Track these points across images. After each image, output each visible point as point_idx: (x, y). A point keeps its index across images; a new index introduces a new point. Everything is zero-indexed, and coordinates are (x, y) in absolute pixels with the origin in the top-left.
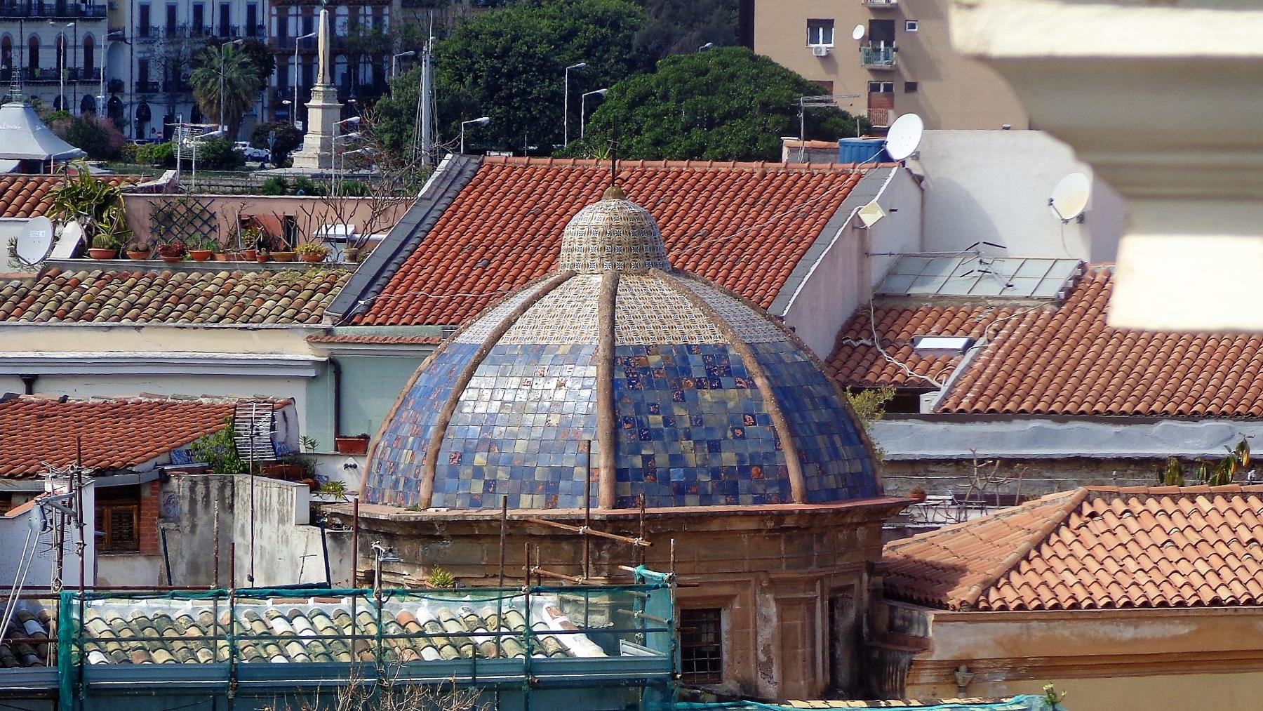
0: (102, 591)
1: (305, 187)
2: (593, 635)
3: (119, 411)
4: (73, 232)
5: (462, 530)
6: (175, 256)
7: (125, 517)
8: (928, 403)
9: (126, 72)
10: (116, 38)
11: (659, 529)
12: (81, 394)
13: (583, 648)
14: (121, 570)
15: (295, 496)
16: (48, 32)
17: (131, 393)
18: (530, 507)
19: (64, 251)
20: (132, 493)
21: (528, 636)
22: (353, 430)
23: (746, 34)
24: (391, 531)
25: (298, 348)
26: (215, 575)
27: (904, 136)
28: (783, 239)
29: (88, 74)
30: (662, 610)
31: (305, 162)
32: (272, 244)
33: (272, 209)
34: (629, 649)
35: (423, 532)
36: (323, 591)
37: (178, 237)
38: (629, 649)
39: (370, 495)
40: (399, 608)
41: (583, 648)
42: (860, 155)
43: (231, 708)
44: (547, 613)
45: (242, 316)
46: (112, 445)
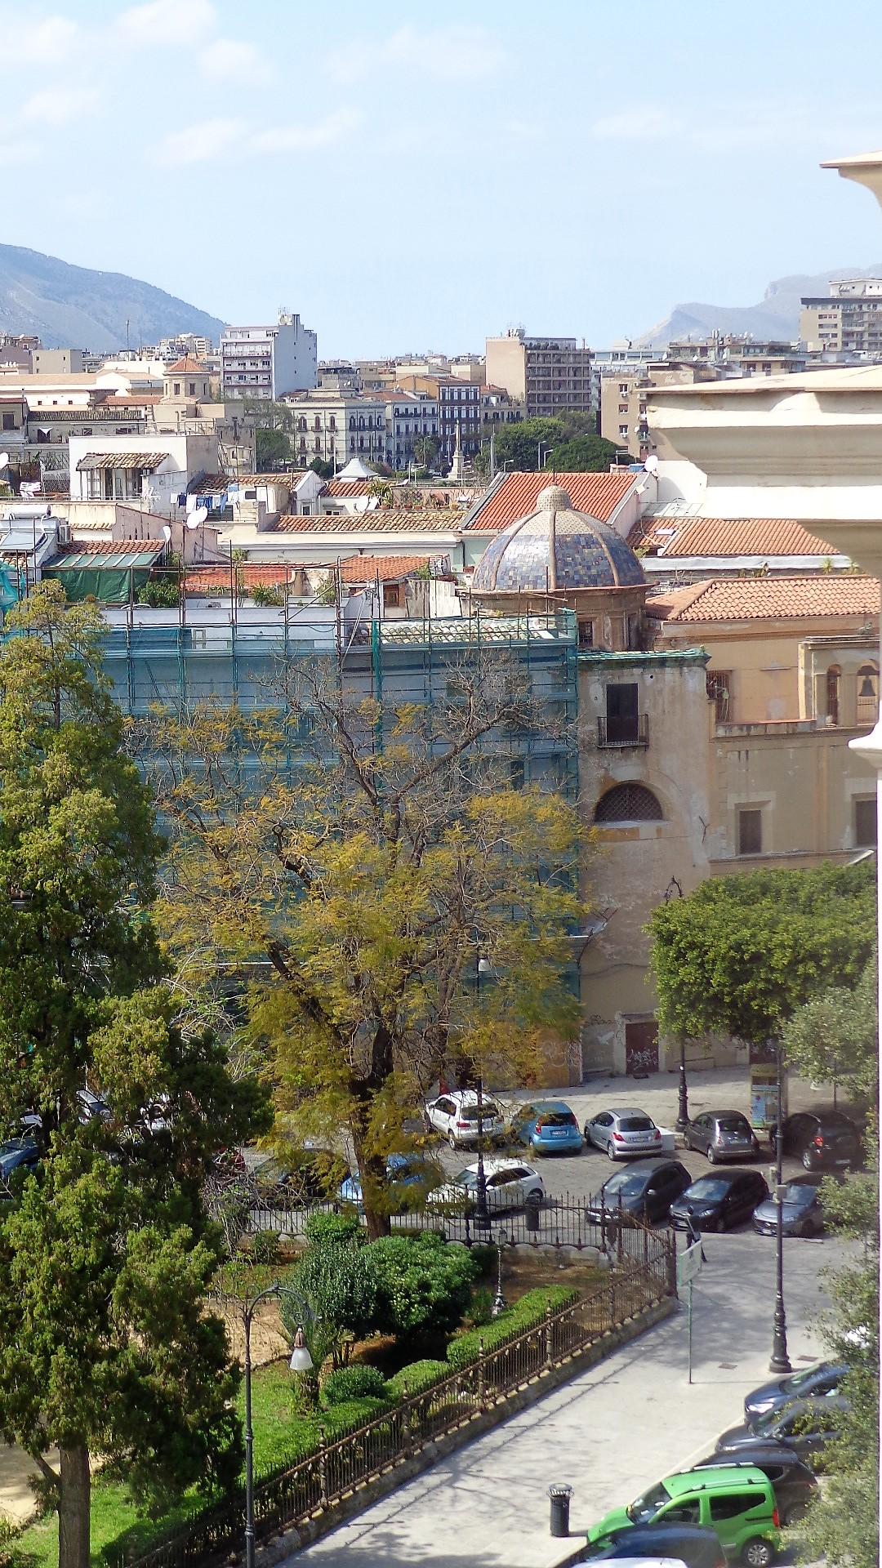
4: (375, 501)
8: (660, 552)
9: (394, 449)
10: (389, 436)
11: (571, 595)
13: (547, 635)
14: (393, 612)
16: (366, 435)
19: (372, 507)
28: (29, 525)
30: (572, 622)
34: (562, 635)
35: (493, 598)
38: (562, 635)
41: (547, 635)
44: (534, 624)
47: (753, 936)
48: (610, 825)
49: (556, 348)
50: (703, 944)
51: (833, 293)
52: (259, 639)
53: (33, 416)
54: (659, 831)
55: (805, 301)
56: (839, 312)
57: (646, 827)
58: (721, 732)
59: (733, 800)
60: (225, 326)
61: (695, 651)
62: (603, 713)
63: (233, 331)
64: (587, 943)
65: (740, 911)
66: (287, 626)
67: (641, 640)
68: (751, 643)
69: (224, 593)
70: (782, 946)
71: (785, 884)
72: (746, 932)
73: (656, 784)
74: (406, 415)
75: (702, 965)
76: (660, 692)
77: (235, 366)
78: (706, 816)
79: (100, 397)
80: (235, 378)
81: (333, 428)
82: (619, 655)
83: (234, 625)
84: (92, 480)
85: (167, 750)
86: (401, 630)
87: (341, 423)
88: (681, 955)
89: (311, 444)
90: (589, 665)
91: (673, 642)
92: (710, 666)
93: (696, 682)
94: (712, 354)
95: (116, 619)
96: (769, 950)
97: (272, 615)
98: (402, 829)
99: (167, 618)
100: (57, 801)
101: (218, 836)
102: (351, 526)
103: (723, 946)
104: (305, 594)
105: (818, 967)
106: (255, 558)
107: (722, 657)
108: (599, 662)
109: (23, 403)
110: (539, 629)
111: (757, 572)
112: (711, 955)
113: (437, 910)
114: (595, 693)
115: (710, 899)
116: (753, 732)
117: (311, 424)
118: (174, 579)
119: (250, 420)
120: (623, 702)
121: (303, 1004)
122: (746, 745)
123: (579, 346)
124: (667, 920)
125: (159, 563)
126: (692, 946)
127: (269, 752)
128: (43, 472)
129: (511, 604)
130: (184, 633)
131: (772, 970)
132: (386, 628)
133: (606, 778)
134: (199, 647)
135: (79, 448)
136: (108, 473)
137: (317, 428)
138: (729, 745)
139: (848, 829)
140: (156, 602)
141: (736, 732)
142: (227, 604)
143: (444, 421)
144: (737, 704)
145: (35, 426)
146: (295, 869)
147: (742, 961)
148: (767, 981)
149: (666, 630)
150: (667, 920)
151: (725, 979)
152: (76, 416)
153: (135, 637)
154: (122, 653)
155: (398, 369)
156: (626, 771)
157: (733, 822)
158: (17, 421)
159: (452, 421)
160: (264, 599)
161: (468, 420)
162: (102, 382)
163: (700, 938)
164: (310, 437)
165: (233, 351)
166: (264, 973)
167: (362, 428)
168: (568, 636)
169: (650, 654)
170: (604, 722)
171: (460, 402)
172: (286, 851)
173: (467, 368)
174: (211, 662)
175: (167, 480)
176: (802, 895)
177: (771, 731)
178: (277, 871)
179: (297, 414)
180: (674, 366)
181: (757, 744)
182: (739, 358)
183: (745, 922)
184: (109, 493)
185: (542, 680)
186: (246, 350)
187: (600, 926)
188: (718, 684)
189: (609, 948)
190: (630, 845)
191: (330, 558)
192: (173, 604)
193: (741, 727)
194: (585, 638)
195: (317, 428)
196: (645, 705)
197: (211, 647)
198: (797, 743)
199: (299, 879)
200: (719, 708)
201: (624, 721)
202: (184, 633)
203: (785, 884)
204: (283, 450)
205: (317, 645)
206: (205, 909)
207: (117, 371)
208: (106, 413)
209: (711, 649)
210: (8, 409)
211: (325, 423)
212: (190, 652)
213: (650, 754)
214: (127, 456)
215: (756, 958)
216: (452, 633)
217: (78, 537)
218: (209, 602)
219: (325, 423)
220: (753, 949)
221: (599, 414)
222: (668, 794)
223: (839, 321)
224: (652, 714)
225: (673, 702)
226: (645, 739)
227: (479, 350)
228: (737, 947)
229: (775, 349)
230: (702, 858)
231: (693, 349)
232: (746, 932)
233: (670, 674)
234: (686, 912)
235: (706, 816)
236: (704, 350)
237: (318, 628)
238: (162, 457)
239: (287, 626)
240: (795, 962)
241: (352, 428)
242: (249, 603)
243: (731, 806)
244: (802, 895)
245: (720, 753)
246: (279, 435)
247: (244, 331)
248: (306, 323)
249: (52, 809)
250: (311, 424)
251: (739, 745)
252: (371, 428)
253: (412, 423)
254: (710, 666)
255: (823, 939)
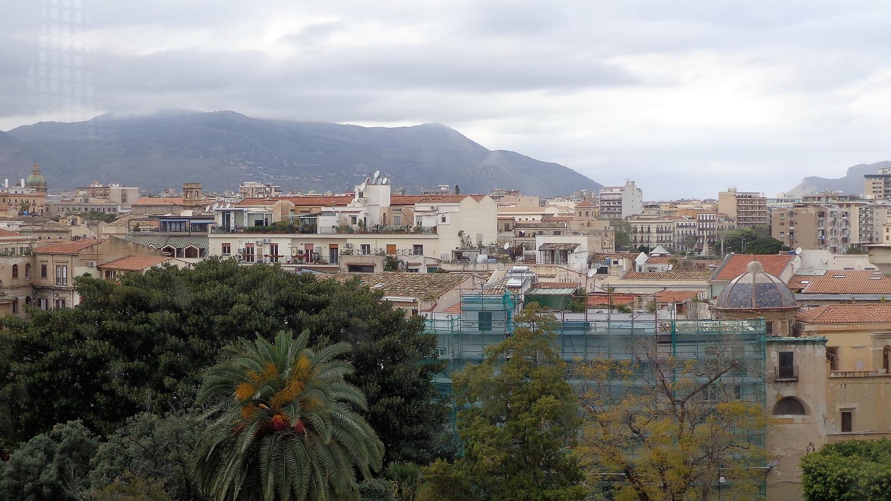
0: (677, 320)
1: (704, 258)
2: (753, 327)
3: (679, 293)
4: (671, 266)
5: (732, 311)
6: (687, 269)
7: (680, 308)
8: (803, 291)
9: (676, 241)
10: (674, 235)
11: (763, 311)
12: (673, 290)
13: (751, 329)
14: (680, 317)
15: (707, 306)
16: (664, 235)
17: (681, 290)
18: (742, 307)
19: (670, 269)
20: (681, 305)
21: (743, 327)
22: (714, 295)
23: (770, 234)
24: (721, 311)
25: (705, 283)
26: (695, 317)
27: (799, 251)
28: (520, 275)
29: (670, 241)
30: (763, 323)
31: (703, 254)
32: (701, 267)
33: (701, 262)
34: (758, 329)
35: (726, 311)
36: (711, 320)
37: (687, 266)
38: (758, 329)
39: (718, 306)
40: (723, 322)
41: (751, 329)
42: (791, 253)
43: (23, 498)
44: (746, 323)
45: (698, 279)
46: (677, 298)
47: (849, 471)
48: (780, 416)
49: (750, 197)
50: (825, 474)
51: (880, 172)
52: (619, 328)
53: (518, 226)
54: (803, 420)
55: (867, 176)
56: (882, 181)
57: (798, 418)
58: (833, 375)
59: (839, 406)
60: (601, 187)
61: (820, 337)
62: (777, 365)
63: (606, 189)
64: (769, 470)
65: (843, 459)
66: (632, 322)
67: (796, 332)
68: (848, 334)
69: (603, 306)
70: (863, 476)
71: (864, 447)
72: (846, 470)
73: (801, 397)
74: (682, 226)
75: (824, 484)
76: (804, 356)
77: (606, 204)
78: (825, 414)
79: (547, 218)
80: (606, 209)
81: (649, 232)
82: (785, 338)
83: (609, 321)
84: (545, 255)
85: (579, 377)
86: (683, 325)
87: (653, 229)
88: (815, 478)
89: (639, 239)
90: (771, 343)
91: (809, 333)
92: (828, 344)
93: (821, 352)
94: (823, 200)
95: (558, 316)
96: (857, 479)
97: (626, 317)
98: (686, 416)
99: (579, 317)
100: (535, 400)
101: (602, 417)
102: (660, 277)
103: (835, 475)
104: (640, 307)
105: (881, 487)
106: (617, 291)
107: (833, 340)
108: (775, 341)
109: (513, 219)
110: (747, 326)
111: (850, 302)
112: (829, 479)
113: (701, 454)
114: (773, 356)
115: (828, 453)
116: (848, 375)
117: (639, 230)
118: (582, 300)
119: (612, 228)
120: (786, 360)
121: (640, 495)
122: (845, 381)
123: (761, 196)
124: (807, 462)
125: (576, 293)
126: (820, 475)
127: (626, 380)
128: (525, 252)
129: (735, 314)
130: (586, 325)
131: (859, 488)
132: (678, 324)
133: (778, 395)
134: (593, 331)
135: (540, 241)
136: (553, 252)
137: (642, 232)
138: (836, 381)
139: (100, 113)
140: (574, 310)
141: (840, 375)
142: (606, 311)
143: (699, 229)
144: (840, 362)
145: (518, 230)
146: (638, 433)
147: (843, 483)
148: (856, 492)
149: (808, 328)
150: (807, 462)
151: (835, 491)
152: (536, 226)
153: (566, 325)
154: (559, 333)
155: (678, 206)
156: (788, 392)
157: (839, 417)
158: (511, 227)
159: (703, 229)
160: (622, 309)
161: (710, 229)
162: (548, 211)
163: (823, 471)
164: (639, 236)
165: (606, 197)
166: (622, 479)
167: (662, 232)
168: (763, 329)
169: (799, 339)
170: (778, 369)
171: (706, 221)
172: (633, 424)
173: (710, 206)
174: (597, 337)
175: (579, 255)
176: (873, 452)
177: (856, 375)
178: (629, 433)
179: (633, 225)
180: (806, 206)
181: (850, 381)
182: (836, 202)
183: (845, 464)
184: (553, 260)
185: (749, 351)
186: (611, 197)
187: (775, 463)
188: (832, 354)
189: (779, 474)
190: (789, 426)
191: (652, 291)
192: (583, 310)
193: (842, 373)
194: (769, 329)
195: (642, 232)
196: (797, 361)
197: (598, 330)
198: (869, 381)
199: (639, 437)
200: (832, 364)
201: (787, 369)
202: (586, 325)
203: (864, 447)
204: (627, 241)
205: (646, 331)
206: (596, 450)
207: (554, 206)
208: (552, 225)
209: (828, 337)
210: (507, 222)
211: (646, 230)
212: (588, 333)
213: (799, 384)
214: (560, 245)
215: (850, 481)
216: (707, 326)
217: (540, 280)
218: (598, 310)
219: (646, 230)
220: (849, 477)
221: (770, 227)
222: (808, 402)
223: (882, 185)
224: (800, 366)
225: (810, 361)
226: (797, 377)
227: (716, 197)
228: (842, 476)
229: (852, 198)
230: (823, 433)
231: (814, 198)
232: (846, 470)
233: (809, 348)
234: (816, 459)
235: (825, 414)
236: (819, 198)
237: (645, 323)
238: (577, 245)
239: (632, 322)
240: (870, 484)
241: (658, 232)
242: (615, 311)
243: (837, 410)
244: (873, 452)
245: (832, 385)
246: (625, 235)
247: (611, 189)
248: (638, 185)
249: (533, 404)
250: (639, 230)
251: (841, 381)
252: (666, 232)
253: (684, 230)
254: (828, 344)
255: (883, 474)
